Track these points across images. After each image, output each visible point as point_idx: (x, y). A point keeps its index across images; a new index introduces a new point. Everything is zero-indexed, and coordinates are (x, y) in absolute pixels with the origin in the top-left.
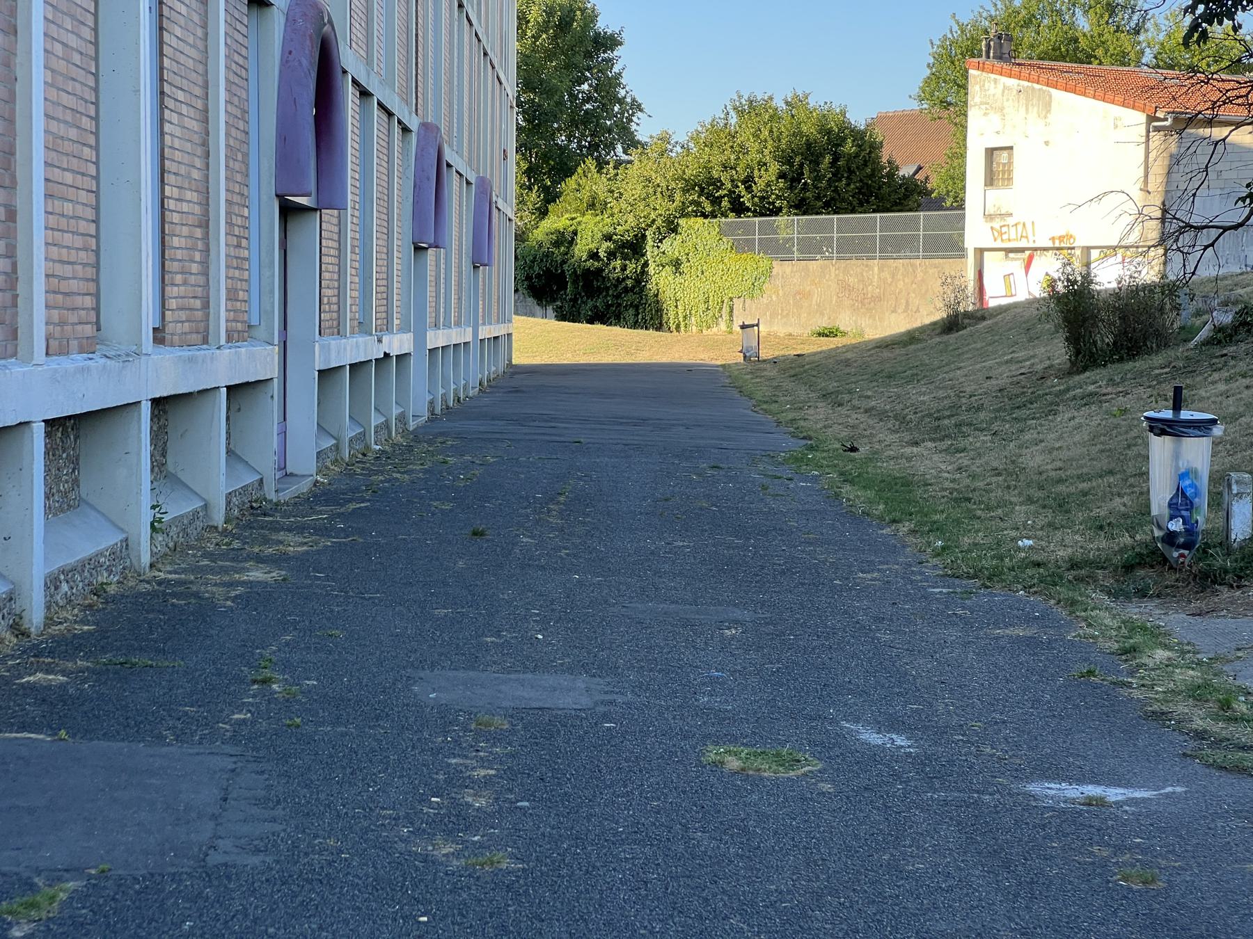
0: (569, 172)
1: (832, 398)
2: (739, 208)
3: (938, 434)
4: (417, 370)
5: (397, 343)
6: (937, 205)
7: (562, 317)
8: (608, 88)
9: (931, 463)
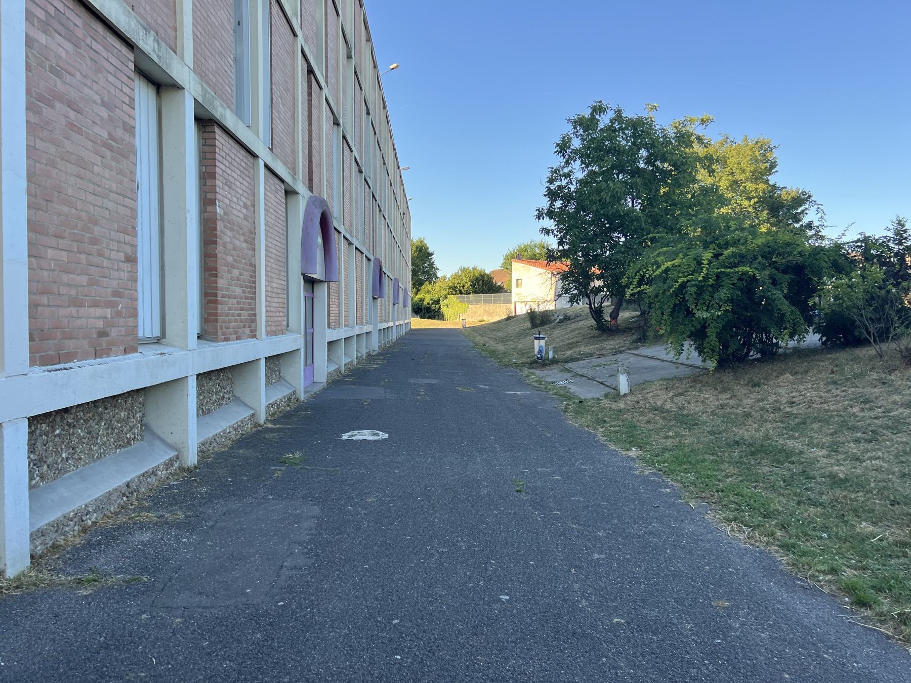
0: (422, 285)
1: (481, 335)
2: (461, 293)
3: (502, 342)
4: (394, 329)
5: (391, 324)
6: (506, 292)
7: (421, 317)
8: (431, 265)
9: (500, 347)
